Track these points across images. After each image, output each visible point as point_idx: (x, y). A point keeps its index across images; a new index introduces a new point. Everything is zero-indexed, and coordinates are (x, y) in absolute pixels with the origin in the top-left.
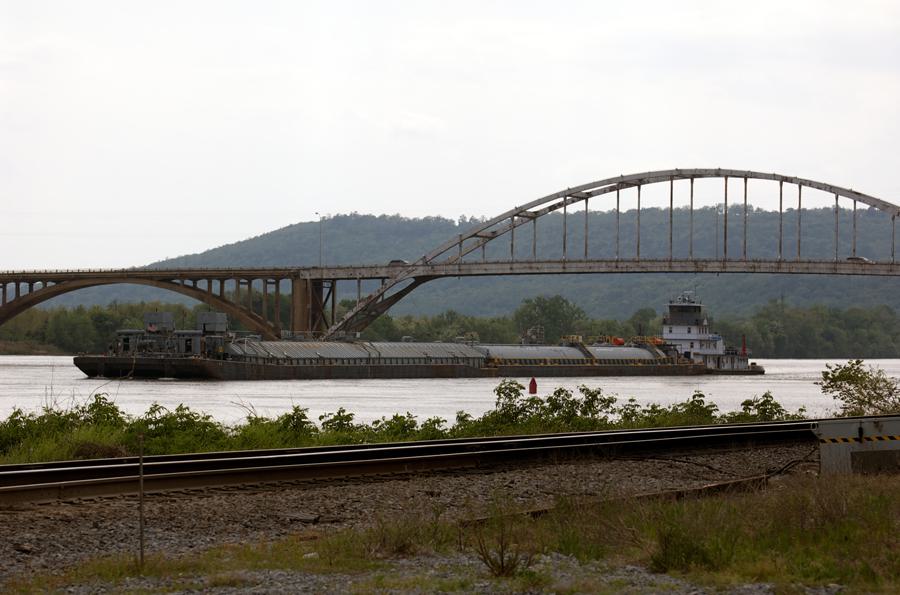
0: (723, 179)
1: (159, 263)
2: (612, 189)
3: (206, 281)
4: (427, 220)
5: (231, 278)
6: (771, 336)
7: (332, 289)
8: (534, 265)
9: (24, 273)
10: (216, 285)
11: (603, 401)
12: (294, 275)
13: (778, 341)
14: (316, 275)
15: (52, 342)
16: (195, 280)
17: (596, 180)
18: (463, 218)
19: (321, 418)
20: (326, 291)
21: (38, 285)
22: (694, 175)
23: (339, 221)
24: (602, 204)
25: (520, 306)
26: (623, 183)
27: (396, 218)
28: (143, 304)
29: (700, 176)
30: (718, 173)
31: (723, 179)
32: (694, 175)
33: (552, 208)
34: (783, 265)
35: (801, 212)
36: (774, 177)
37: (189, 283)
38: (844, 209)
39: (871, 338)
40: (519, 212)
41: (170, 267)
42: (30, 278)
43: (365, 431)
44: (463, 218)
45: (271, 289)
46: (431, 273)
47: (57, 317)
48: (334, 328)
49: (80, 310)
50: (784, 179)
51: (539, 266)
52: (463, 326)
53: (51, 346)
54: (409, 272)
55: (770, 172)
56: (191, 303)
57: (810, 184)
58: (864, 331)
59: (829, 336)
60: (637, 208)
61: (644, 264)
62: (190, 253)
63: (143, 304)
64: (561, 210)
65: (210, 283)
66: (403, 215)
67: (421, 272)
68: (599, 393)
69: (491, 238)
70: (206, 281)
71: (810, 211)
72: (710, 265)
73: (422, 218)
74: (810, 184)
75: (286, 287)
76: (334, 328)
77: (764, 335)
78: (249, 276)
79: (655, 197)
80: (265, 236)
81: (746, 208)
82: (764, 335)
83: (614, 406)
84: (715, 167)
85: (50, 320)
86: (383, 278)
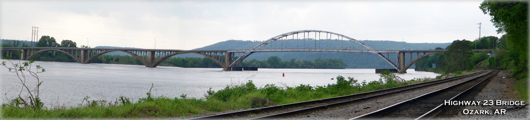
0: (315, 32)
1: (201, 48)
2: (292, 34)
3: (135, 52)
4: (247, 41)
5: (224, 52)
6: (318, 64)
7: (234, 54)
8: (276, 50)
9: (169, 50)
10: (209, 53)
11: (354, 81)
12: (226, 52)
13: (320, 65)
14: (230, 51)
15: (173, 64)
16: (131, 51)
17: (289, 32)
18: (255, 41)
19: (249, 81)
20: (232, 55)
21: (172, 53)
22: (297, 33)
23: (230, 41)
24: (290, 37)
25: (268, 58)
26: (294, 33)
27: (241, 41)
28: (192, 57)
29: (310, 32)
30: (314, 31)
31: (315, 32)
32: (297, 33)
33: (279, 38)
34: (327, 50)
35: (330, 40)
36: (326, 32)
37: (130, 52)
38: (362, 41)
39: (338, 65)
40: (273, 39)
41: (196, 50)
42: (171, 51)
43: (358, 88)
44: (255, 41)
45: (221, 54)
46: (254, 51)
47: (174, 59)
48: (234, 62)
49: (179, 58)
50: (328, 32)
51: (277, 50)
52: (257, 62)
53: (173, 65)
54: (250, 51)
55: (325, 31)
56: (130, 55)
57: (333, 33)
58: (336, 63)
59: (330, 64)
60: (292, 38)
61: (299, 49)
62: (200, 47)
63: (192, 57)
64: (281, 39)
65: (208, 53)
66: (243, 40)
67: (252, 51)
68: (353, 79)
69: (267, 44)
70: (135, 52)
71: (462, 41)
72: (312, 50)
73: (246, 41)
74: (333, 33)
75: (224, 54)
76: (234, 62)
77: (317, 64)
78: (216, 52)
79: (301, 36)
80: (215, 44)
81: (342, 40)
82: (317, 64)
83: (357, 82)
84: (313, 30)
85: (173, 60)
86: (244, 52)
